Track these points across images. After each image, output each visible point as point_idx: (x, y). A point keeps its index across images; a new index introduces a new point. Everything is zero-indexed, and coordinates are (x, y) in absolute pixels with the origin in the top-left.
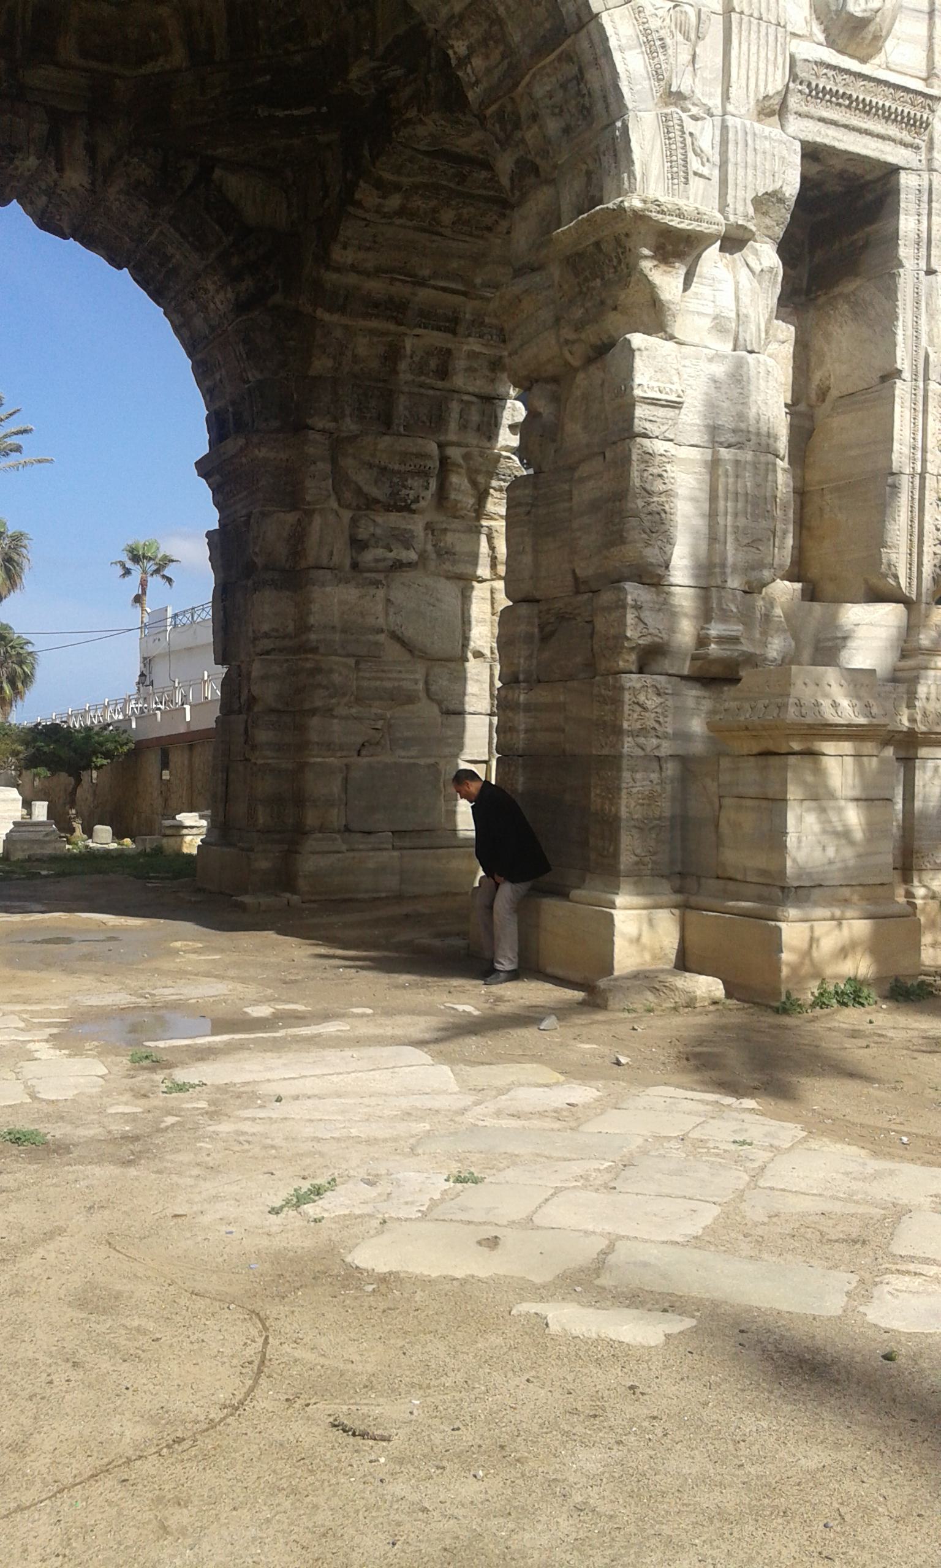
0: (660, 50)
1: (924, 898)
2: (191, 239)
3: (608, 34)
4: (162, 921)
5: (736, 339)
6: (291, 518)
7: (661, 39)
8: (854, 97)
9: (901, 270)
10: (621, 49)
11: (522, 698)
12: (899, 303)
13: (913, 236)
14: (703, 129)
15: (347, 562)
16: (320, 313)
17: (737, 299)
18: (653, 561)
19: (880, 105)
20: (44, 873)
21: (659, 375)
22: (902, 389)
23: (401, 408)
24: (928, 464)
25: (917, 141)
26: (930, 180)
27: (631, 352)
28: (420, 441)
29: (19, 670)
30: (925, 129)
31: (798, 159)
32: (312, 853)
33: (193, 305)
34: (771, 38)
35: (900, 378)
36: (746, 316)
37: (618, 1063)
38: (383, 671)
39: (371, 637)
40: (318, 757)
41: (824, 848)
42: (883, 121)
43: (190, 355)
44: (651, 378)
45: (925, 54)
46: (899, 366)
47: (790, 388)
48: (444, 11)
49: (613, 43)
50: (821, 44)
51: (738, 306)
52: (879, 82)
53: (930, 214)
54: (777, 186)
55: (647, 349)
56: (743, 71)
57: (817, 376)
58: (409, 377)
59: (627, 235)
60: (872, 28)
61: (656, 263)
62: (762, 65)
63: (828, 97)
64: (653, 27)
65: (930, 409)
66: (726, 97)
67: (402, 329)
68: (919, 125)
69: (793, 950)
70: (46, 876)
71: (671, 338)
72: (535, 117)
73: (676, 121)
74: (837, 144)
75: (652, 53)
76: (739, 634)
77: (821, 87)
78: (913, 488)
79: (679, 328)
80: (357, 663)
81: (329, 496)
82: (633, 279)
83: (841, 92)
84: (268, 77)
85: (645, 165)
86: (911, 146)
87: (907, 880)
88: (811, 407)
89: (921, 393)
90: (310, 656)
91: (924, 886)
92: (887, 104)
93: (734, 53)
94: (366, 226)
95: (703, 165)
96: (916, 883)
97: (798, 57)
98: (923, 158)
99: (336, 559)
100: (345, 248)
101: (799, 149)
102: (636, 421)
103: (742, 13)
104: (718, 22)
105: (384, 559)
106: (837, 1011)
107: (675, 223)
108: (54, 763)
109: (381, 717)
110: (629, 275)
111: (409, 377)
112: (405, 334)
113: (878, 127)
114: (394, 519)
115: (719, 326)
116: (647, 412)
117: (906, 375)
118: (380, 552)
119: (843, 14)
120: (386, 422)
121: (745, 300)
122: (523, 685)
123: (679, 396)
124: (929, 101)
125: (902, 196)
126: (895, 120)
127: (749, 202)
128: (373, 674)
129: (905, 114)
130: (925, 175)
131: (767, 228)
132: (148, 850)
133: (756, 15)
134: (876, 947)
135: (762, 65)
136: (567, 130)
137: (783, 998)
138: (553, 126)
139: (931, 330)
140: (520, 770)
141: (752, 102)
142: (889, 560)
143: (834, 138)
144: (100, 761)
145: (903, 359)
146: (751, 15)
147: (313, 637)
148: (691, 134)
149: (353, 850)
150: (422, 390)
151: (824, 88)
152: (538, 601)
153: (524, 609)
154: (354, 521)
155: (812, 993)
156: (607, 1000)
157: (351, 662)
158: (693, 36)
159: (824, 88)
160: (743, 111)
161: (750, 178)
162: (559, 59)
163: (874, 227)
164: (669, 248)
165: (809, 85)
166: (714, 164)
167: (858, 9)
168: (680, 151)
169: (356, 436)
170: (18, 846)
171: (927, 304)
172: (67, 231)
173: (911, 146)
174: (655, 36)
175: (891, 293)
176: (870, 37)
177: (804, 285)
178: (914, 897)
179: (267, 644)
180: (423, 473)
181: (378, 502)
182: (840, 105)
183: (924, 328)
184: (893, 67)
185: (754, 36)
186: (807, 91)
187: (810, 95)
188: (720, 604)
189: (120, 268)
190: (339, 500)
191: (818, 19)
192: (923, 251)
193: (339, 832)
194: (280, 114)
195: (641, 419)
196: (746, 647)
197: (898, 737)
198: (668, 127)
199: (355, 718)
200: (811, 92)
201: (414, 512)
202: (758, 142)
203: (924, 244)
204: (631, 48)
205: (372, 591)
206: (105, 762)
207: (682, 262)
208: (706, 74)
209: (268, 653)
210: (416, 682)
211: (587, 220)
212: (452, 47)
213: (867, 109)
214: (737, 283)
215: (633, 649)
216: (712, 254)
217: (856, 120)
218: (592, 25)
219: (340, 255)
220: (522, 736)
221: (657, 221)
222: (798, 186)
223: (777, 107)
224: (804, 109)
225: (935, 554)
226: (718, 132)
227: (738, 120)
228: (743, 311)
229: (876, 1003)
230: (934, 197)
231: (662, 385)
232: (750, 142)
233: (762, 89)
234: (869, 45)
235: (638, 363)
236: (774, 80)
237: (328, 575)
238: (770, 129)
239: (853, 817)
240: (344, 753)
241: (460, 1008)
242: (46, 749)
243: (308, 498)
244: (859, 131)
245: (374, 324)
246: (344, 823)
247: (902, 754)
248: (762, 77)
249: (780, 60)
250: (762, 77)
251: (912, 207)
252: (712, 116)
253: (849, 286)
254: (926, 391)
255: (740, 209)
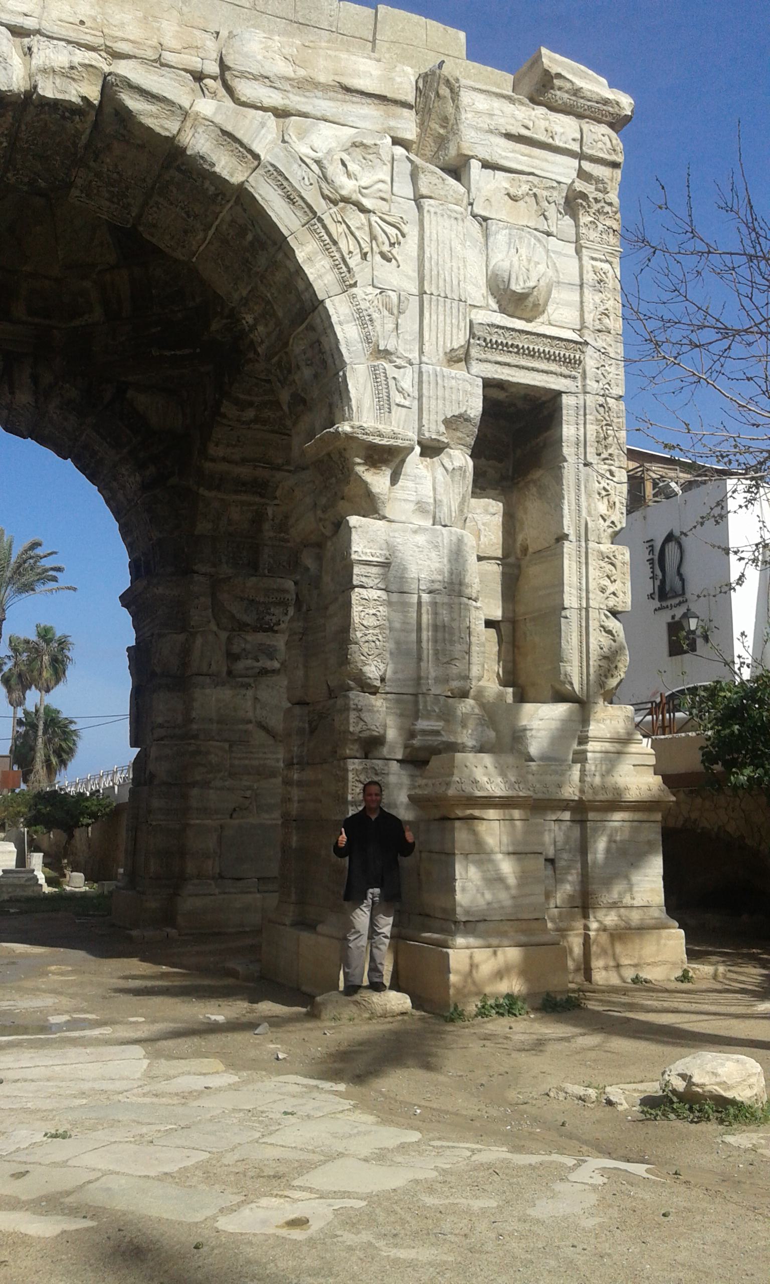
0: (369, 323)
1: (598, 930)
2: (108, 440)
3: (331, 313)
4: (62, 950)
5: (434, 518)
6: (181, 637)
7: (369, 315)
8: (521, 346)
9: (565, 464)
10: (340, 323)
11: (296, 777)
12: (565, 487)
13: (573, 439)
14: (405, 374)
15: (225, 669)
16: (202, 491)
17: (434, 489)
18: (371, 676)
19: (541, 350)
20: (12, 911)
21: (371, 544)
22: (568, 548)
23: (266, 556)
24: (591, 601)
25: (573, 373)
26: (585, 400)
27: (349, 529)
28: (279, 580)
29: (64, 745)
30: (579, 365)
31: (480, 391)
32: (190, 895)
33: (115, 484)
34: (455, 311)
35: (567, 540)
36: (440, 501)
37: (278, 1059)
38: (251, 752)
39: (241, 727)
40: (197, 819)
41: (483, 894)
42: (545, 361)
43: (117, 520)
44: (365, 547)
45: (578, 313)
46: (566, 531)
47: (501, 546)
48: (236, 296)
49: (334, 319)
50: (495, 311)
51: (435, 494)
52: (538, 335)
53: (585, 424)
54: (462, 410)
55: (360, 527)
56: (434, 333)
57: (520, 538)
58: (272, 534)
59: (345, 449)
60: (531, 299)
61: (367, 467)
62: (448, 328)
63: (500, 347)
64: (363, 307)
65: (590, 561)
66: (421, 352)
67: (263, 500)
68: (574, 363)
69: (458, 972)
70: (13, 914)
71: (384, 518)
72: (298, 367)
73: (381, 371)
74: (510, 379)
75: (363, 325)
76: (439, 728)
77: (494, 341)
78: (581, 618)
79: (388, 512)
80: (231, 746)
81: (209, 622)
82: (352, 479)
83: (510, 343)
84: (159, 328)
85: (359, 401)
86: (570, 377)
87: (586, 916)
88: (517, 559)
89: (583, 550)
90: (193, 741)
91: (598, 921)
92: (547, 350)
93: (426, 321)
94: (232, 430)
95: (405, 398)
96: (592, 918)
97: (475, 322)
98: (579, 384)
99: (214, 667)
100: (217, 445)
101: (481, 384)
102: (355, 577)
103: (432, 294)
104: (414, 302)
105: (253, 668)
106: (495, 1020)
107: (377, 440)
108: (49, 823)
109: (249, 788)
110: (349, 476)
111: (272, 534)
112: (267, 504)
113: (543, 365)
114: (261, 637)
115: (421, 508)
116: (363, 570)
117: (572, 537)
118: (249, 662)
119: (508, 292)
120: (254, 567)
121: (440, 490)
122: (296, 767)
123: (387, 559)
124: (579, 346)
125: (564, 412)
126: (555, 360)
127: (440, 423)
128: (244, 755)
129: (562, 355)
130: (581, 396)
131: (459, 438)
132: (106, 892)
133: (443, 295)
134: (526, 971)
135: (448, 328)
136: (316, 376)
137: (452, 1009)
138: (307, 372)
139: (589, 505)
140: (294, 831)
141: (441, 354)
142: (566, 671)
143: (508, 375)
144: (86, 821)
145: (569, 527)
146: (439, 295)
147: (195, 726)
148: (394, 378)
149: (225, 893)
150: (282, 543)
151: (496, 341)
152: (308, 704)
153: (297, 710)
154: (229, 640)
155: (476, 1006)
156: (320, 1012)
157: (226, 746)
158: (395, 312)
159: (496, 341)
160: (434, 361)
161: (441, 406)
162: (307, 328)
163: (548, 433)
164: (376, 457)
165: (485, 340)
166: (414, 398)
167: (518, 287)
168: (384, 390)
169: (230, 578)
170: (4, 889)
171: (586, 487)
172: (25, 433)
173: (570, 377)
174: (365, 313)
175: (559, 479)
176: (531, 305)
177: (510, 474)
178: (589, 930)
179: (161, 732)
180: (284, 604)
181: (248, 625)
182: (511, 352)
183: (584, 504)
184: (554, 323)
185: (441, 309)
186: (484, 344)
187: (486, 346)
188: (425, 706)
189: (65, 458)
190: (218, 625)
191: (492, 294)
192: (582, 450)
193: (213, 878)
194: (167, 353)
195: (358, 575)
196: (446, 738)
197: (572, 804)
198: (375, 374)
199: (228, 789)
200: (487, 344)
201: (276, 632)
202: (446, 381)
203: (582, 445)
204: (348, 322)
205: (243, 691)
206: (90, 821)
207: (387, 466)
208: (407, 337)
209: (162, 739)
210: (278, 760)
211: (320, 438)
212: (244, 318)
213: (532, 354)
214: (434, 479)
215: (356, 740)
216: (414, 457)
217: (523, 362)
218: (320, 308)
219: (213, 450)
220: (296, 805)
221: (363, 440)
222: (481, 409)
223: (463, 356)
224: (483, 356)
225: (600, 666)
226: (416, 376)
227: (430, 367)
228: (438, 497)
229: (527, 1013)
230: (587, 411)
231: (373, 551)
232: (440, 381)
233: (449, 345)
234: (532, 310)
235: (354, 536)
236: (459, 338)
237: (208, 680)
238: (458, 372)
239: (507, 867)
240: (219, 816)
241: (213, 1017)
242: (44, 811)
243: (192, 623)
244: (527, 368)
245: (244, 497)
246: (218, 871)
247: (578, 817)
248: (448, 336)
249: (462, 324)
250: (448, 336)
251: (572, 419)
252: (411, 364)
253: (537, 474)
254: (587, 548)
255: (433, 427)
